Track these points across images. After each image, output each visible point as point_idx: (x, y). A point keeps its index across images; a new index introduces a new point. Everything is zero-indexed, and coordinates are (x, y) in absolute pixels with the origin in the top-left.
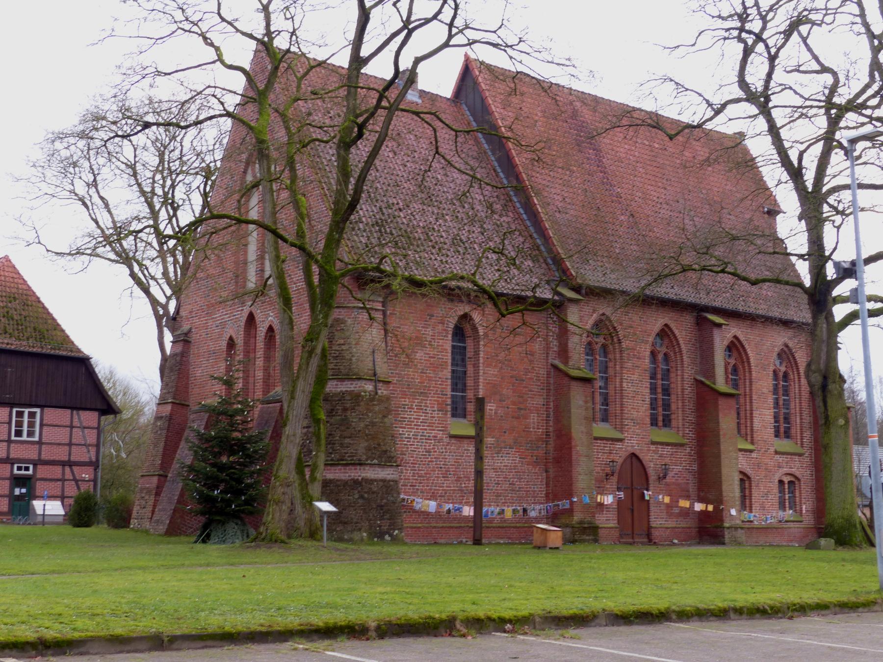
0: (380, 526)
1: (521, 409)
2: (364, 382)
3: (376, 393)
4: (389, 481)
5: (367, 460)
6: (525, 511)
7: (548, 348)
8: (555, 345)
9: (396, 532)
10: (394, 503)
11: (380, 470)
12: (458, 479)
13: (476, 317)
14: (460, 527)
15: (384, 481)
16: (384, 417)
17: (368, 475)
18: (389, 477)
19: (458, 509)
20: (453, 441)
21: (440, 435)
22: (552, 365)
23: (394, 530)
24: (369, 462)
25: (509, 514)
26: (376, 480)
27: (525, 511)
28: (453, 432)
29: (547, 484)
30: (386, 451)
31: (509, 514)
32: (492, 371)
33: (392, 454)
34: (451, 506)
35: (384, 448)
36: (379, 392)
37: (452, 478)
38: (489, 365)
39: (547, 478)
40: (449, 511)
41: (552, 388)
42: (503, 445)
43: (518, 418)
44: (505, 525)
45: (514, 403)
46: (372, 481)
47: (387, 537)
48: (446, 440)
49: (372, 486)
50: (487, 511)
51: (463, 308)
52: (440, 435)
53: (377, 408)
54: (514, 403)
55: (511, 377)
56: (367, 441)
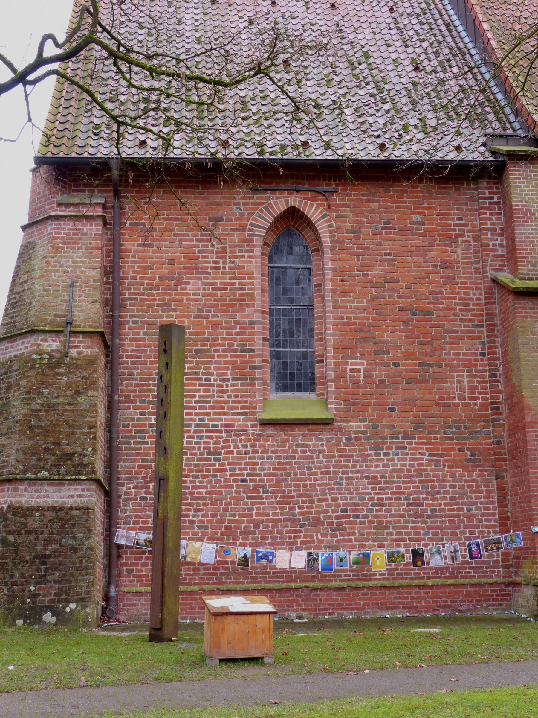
0: (34, 596)
1: (429, 365)
2: (43, 336)
3: (66, 355)
4: (71, 508)
5: (25, 472)
6: (417, 555)
7: (483, 248)
8: (496, 242)
9: (73, 606)
10: (75, 550)
11: (51, 489)
12: (285, 500)
13: (313, 211)
14: (288, 589)
15: (57, 509)
16: (78, 393)
17: (23, 500)
18: (70, 502)
19: (266, 556)
20: (269, 431)
21: (239, 422)
22: (494, 280)
23: (68, 602)
24: (29, 475)
25: (379, 561)
26: (39, 509)
27: (417, 555)
28: (266, 416)
29: (502, 503)
30: (70, 456)
31: (379, 561)
32: (355, 305)
33: (85, 460)
34: (248, 550)
35: (68, 449)
36: (73, 352)
37: (268, 499)
38: (346, 293)
39: (501, 489)
40: (245, 561)
41: (497, 321)
42: (387, 432)
43: (423, 381)
44: (397, 583)
45: (410, 356)
46: (30, 511)
47: (48, 617)
48: (253, 431)
49: (29, 520)
50: (330, 559)
51: (279, 202)
52: (239, 422)
53: (64, 380)
54: (410, 356)
55: (401, 309)
56: (30, 438)
